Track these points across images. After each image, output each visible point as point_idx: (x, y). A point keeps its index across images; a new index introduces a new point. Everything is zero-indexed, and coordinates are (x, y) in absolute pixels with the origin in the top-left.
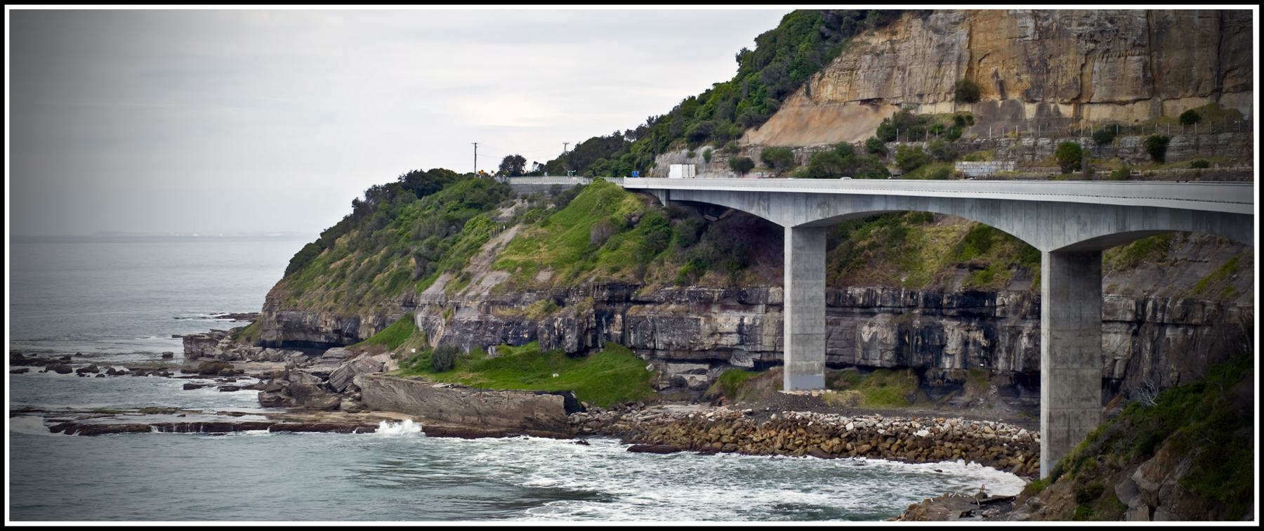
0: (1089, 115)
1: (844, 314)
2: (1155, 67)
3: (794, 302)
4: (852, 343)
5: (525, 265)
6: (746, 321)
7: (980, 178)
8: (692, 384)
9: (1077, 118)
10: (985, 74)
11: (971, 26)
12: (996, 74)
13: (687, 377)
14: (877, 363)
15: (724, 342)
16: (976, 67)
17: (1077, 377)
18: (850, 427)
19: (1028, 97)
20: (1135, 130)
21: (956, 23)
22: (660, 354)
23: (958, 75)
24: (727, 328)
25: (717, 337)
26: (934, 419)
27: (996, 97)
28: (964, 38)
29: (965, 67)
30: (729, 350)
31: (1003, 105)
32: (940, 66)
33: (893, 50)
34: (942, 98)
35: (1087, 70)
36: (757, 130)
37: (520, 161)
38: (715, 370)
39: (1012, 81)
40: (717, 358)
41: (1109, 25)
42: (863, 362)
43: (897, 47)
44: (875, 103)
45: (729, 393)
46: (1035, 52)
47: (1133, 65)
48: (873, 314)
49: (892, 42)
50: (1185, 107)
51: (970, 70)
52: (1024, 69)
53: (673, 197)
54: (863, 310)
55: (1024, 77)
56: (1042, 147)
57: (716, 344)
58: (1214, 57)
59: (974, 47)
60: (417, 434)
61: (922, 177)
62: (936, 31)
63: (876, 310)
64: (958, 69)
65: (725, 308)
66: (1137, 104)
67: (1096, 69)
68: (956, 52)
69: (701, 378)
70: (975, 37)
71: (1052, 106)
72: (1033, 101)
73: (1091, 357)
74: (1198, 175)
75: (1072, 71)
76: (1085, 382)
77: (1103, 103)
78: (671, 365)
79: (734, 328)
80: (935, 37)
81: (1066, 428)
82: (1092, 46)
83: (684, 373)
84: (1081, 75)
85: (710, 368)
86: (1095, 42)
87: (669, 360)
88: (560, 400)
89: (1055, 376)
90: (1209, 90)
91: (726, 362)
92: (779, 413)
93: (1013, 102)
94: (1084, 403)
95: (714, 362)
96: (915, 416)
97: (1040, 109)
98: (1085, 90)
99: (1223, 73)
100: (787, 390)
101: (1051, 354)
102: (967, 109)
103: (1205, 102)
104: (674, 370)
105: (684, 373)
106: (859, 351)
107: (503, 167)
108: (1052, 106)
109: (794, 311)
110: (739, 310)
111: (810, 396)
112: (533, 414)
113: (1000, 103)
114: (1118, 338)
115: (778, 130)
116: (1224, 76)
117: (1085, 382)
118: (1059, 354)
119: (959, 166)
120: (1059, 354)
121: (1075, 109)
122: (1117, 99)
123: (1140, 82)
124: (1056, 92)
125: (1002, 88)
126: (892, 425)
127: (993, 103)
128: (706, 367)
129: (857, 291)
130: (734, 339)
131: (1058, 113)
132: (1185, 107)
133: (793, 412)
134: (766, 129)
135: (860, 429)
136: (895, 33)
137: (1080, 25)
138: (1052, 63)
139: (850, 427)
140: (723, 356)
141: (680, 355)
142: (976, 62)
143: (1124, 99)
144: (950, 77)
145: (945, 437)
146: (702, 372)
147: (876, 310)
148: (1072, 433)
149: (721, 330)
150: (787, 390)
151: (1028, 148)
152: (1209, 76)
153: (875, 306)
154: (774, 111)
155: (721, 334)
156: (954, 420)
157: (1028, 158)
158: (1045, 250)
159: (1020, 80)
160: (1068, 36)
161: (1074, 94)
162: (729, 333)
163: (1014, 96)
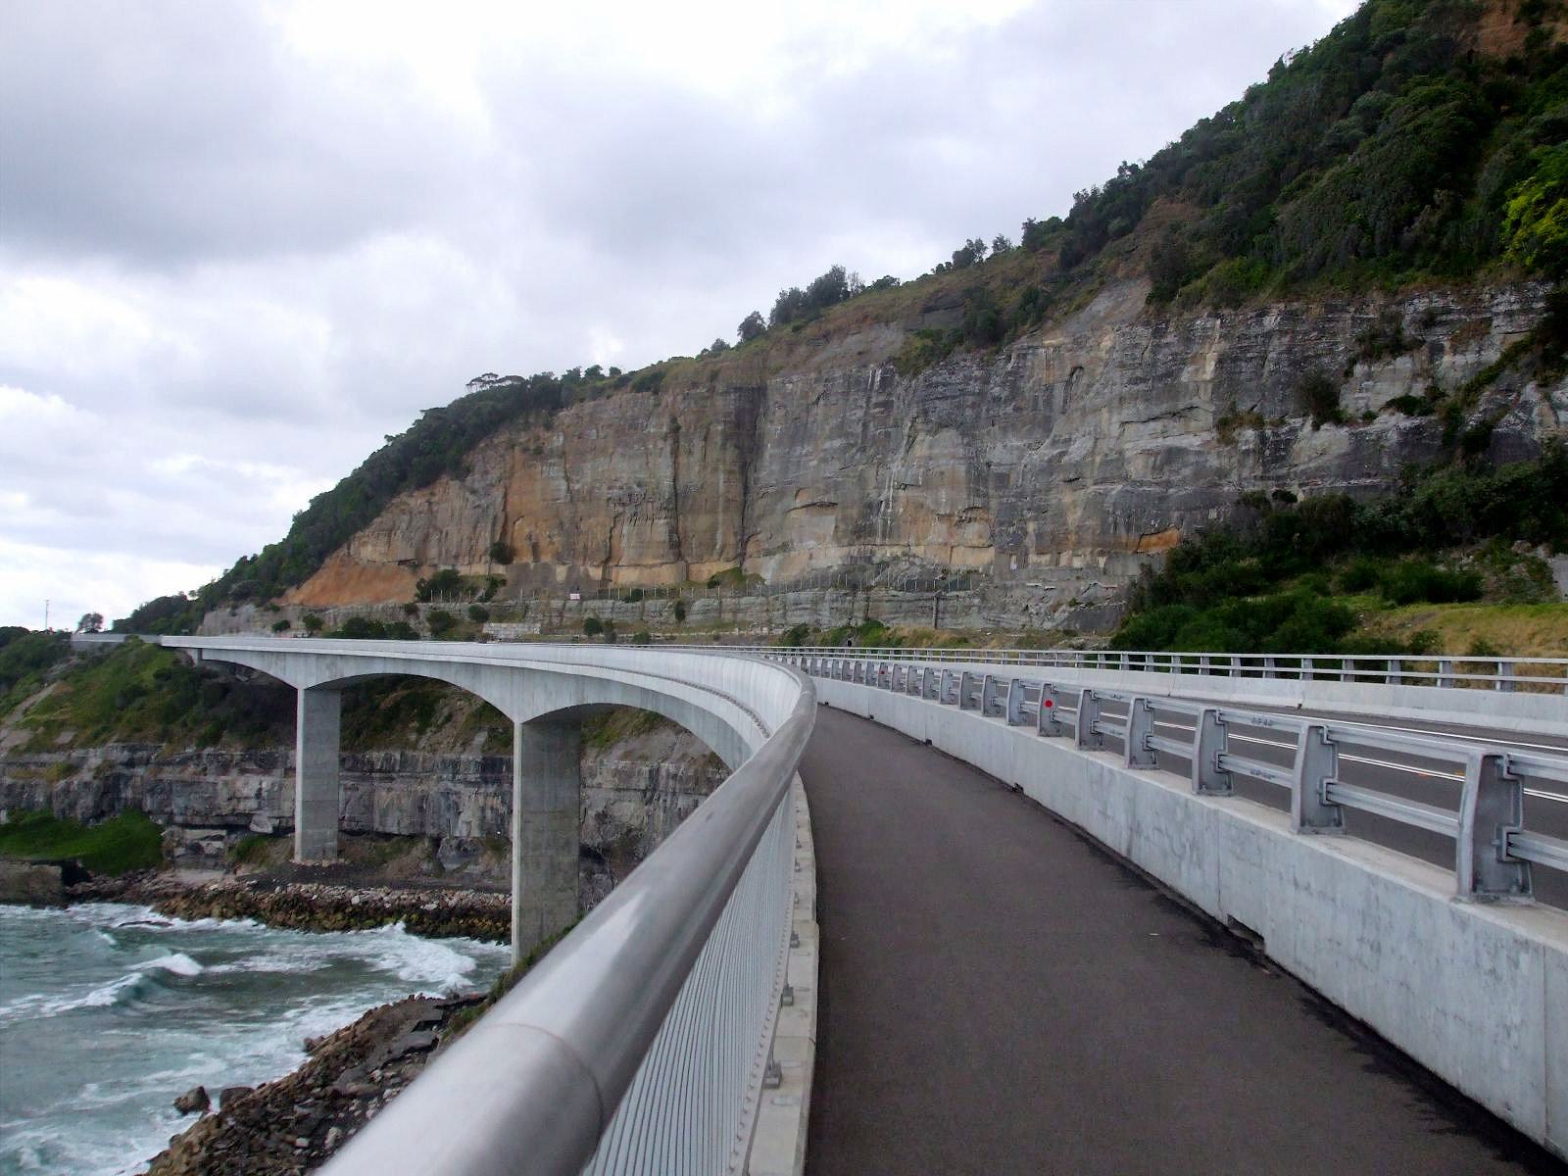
0: (617, 578)
1: (363, 779)
2: (680, 530)
3: (305, 766)
4: (369, 808)
5: (48, 725)
6: (264, 785)
7: (507, 640)
8: (208, 851)
9: (605, 580)
10: (521, 531)
11: (506, 488)
12: (530, 537)
13: (204, 844)
14: (394, 830)
15: (242, 807)
16: (510, 529)
17: (552, 865)
18: (356, 900)
19: (559, 558)
20: (660, 593)
21: (493, 486)
22: (179, 819)
23: (493, 536)
24: (246, 792)
25: (235, 801)
26: (444, 892)
27: (528, 559)
28: (499, 500)
29: (499, 529)
30: (249, 816)
31: (535, 567)
32: (475, 528)
33: (430, 511)
34: (477, 559)
35: (616, 532)
36: (298, 588)
37: (97, 619)
38: (233, 836)
39: (543, 543)
40: (236, 824)
41: (638, 489)
42: (381, 829)
43: (435, 508)
44: (414, 565)
45: (244, 855)
46: (566, 513)
47: (660, 529)
48: (392, 779)
49: (430, 503)
50: (710, 571)
51: (504, 532)
52: (556, 532)
53: (205, 656)
54: (383, 775)
55: (555, 539)
56: (570, 610)
57: (234, 810)
58: (737, 521)
59: (509, 509)
60: (54, 877)
61: (452, 639)
62: (474, 492)
63: (394, 775)
64: (493, 530)
65: (243, 771)
66: (663, 567)
67: (624, 532)
68: (491, 512)
69: (218, 844)
70: (510, 499)
71: (582, 568)
72: (564, 564)
73: (568, 843)
74: (717, 638)
75: (601, 535)
76: (560, 870)
77: (629, 566)
78: (188, 831)
79: (253, 794)
80: (472, 498)
81: (539, 923)
82: (621, 509)
83: (202, 839)
84: (611, 537)
85: (229, 834)
86: (624, 505)
87: (186, 825)
88: (56, 871)
89: (526, 864)
90: (731, 554)
91: (246, 828)
92: (284, 887)
93: (545, 564)
94: (559, 894)
95: (231, 828)
96: (425, 888)
97: (571, 570)
98: (614, 553)
99: (746, 537)
100: (298, 859)
101: (522, 840)
102: (500, 570)
103: (729, 566)
104: (192, 835)
105: (202, 839)
106: (377, 817)
107: (81, 625)
108: (582, 568)
109: (305, 776)
110: (258, 774)
111: (320, 866)
112: (28, 885)
113: (532, 565)
114: (633, 805)
115: (318, 588)
116: (748, 540)
117: (560, 870)
118: (531, 838)
119: (489, 628)
120: (531, 838)
121: (604, 572)
122: (644, 563)
123: (667, 545)
124: (586, 555)
125: (536, 550)
126: (399, 898)
127: (527, 565)
128: (224, 833)
129: (375, 754)
130: (252, 804)
131: (588, 576)
132: (710, 571)
133: (298, 885)
134: (307, 588)
135: (366, 902)
136: (432, 494)
137: (609, 488)
138: (583, 527)
139: (356, 900)
140: (242, 821)
141: (197, 820)
142: (510, 524)
143: (651, 562)
144: (484, 542)
145: (452, 911)
146: (220, 838)
147: (394, 775)
148: (545, 928)
149: (238, 795)
150: (298, 859)
151: (557, 610)
152: (732, 540)
153: (393, 771)
154: (315, 570)
155: (239, 799)
156: (464, 893)
157: (556, 621)
158: (518, 721)
159: (552, 543)
160: (599, 499)
161: (603, 557)
162: (246, 798)
163: (546, 558)
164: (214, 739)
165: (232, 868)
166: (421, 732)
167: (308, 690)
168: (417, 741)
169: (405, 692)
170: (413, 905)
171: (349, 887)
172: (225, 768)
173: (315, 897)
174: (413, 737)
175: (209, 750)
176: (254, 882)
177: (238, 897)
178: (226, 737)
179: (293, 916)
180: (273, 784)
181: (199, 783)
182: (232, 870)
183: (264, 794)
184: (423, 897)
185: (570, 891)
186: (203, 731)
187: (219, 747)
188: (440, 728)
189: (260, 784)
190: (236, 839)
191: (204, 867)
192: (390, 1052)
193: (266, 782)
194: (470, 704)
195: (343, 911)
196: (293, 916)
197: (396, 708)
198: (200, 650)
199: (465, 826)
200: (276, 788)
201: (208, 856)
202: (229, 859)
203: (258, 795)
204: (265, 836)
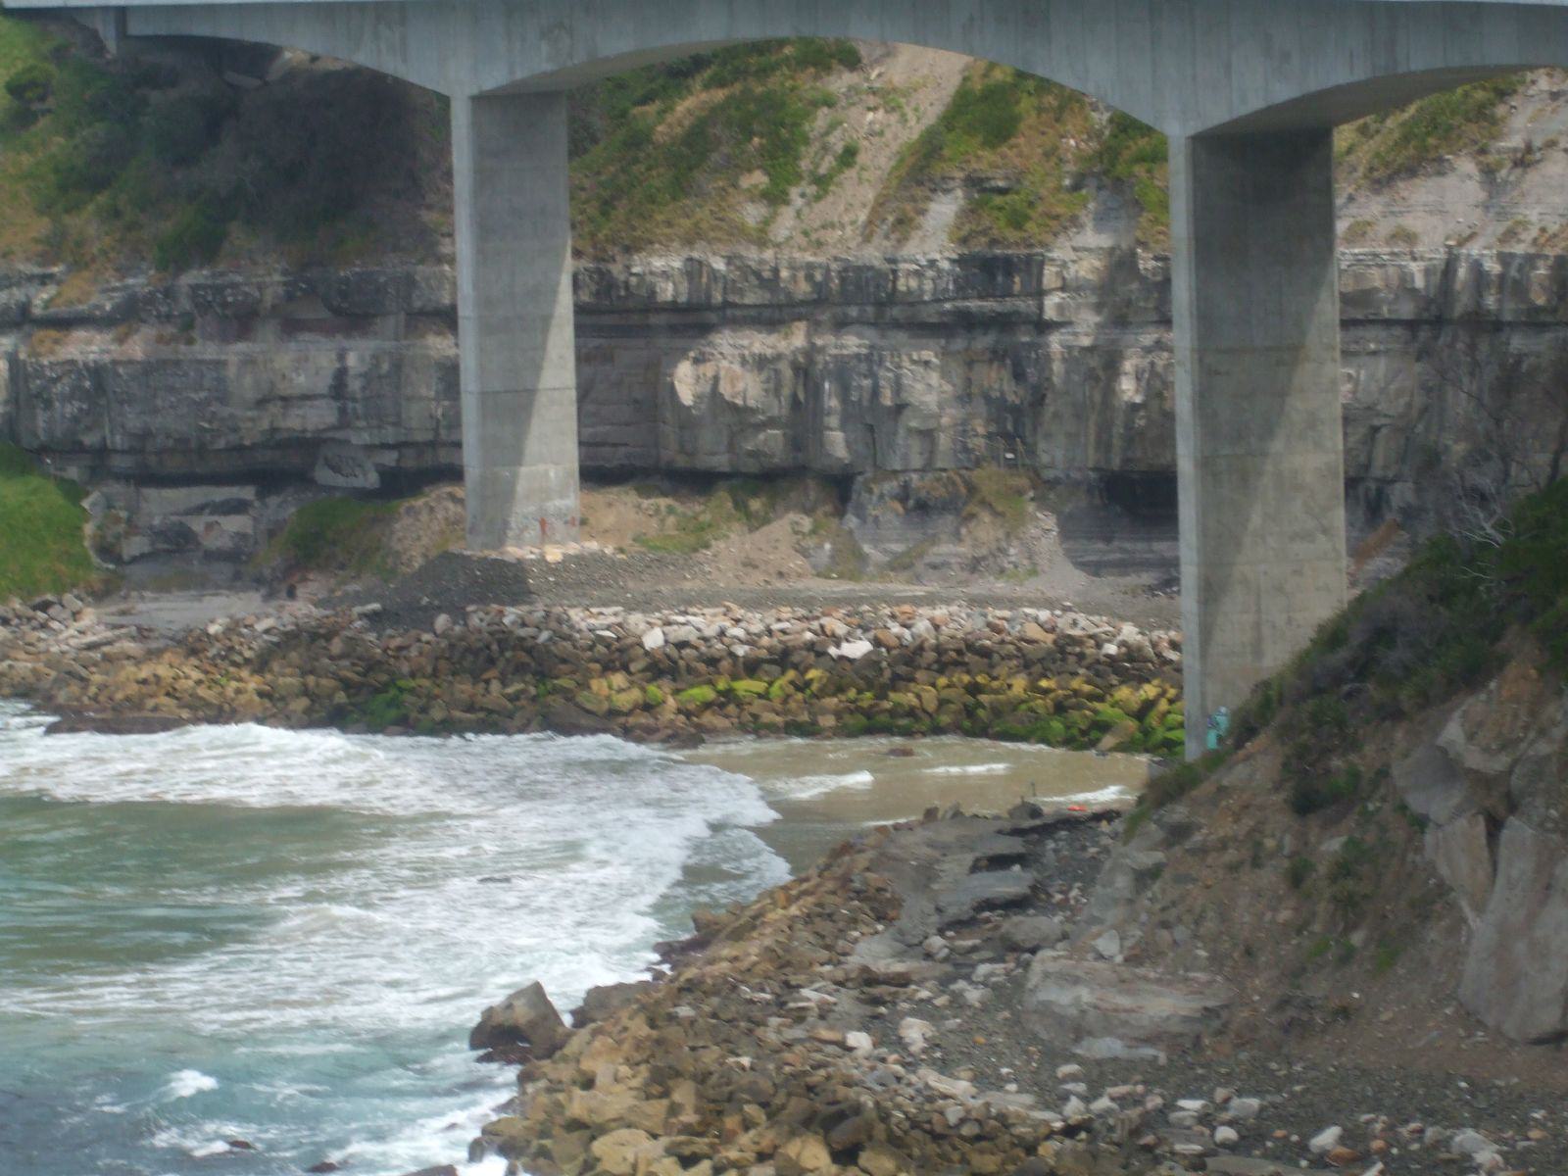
6: (352, 360)
8: (213, 542)
13: (197, 525)
24: (301, 382)
38: (273, 501)
42: (681, 462)
53: (136, 28)
54: (675, 319)
69: (234, 524)
78: (151, 493)
79: (323, 384)
83: (189, 512)
92: (459, 614)
105: (189, 512)
111: (542, 560)
128: (247, 493)
146: (238, 507)
149: (283, 389)
164: (204, 246)
165: (279, 585)
166: (775, 198)
167: (481, 101)
168: (766, 222)
169: (719, 95)
170: (810, 646)
171: (630, 608)
172: (242, 321)
173: (544, 636)
174: (752, 214)
175: (195, 276)
176: (376, 606)
177: (337, 646)
178: (238, 235)
179: (495, 686)
180: (376, 359)
181: (177, 363)
182: (284, 587)
183: (355, 385)
184: (836, 625)
185: (1321, 538)
186: (167, 227)
187: (221, 267)
188: (822, 182)
189: (341, 357)
190: (285, 508)
191: (200, 585)
192: (939, 910)
193: (358, 355)
194: (904, 120)
195: (625, 668)
196: (495, 686)
197: (697, 140)
198: (122, 12)
199: (916, 445)
200: (385, 367)
201: (211, 556)
202: (271, 559)
203: (339, 388)
204: (364, 495)
